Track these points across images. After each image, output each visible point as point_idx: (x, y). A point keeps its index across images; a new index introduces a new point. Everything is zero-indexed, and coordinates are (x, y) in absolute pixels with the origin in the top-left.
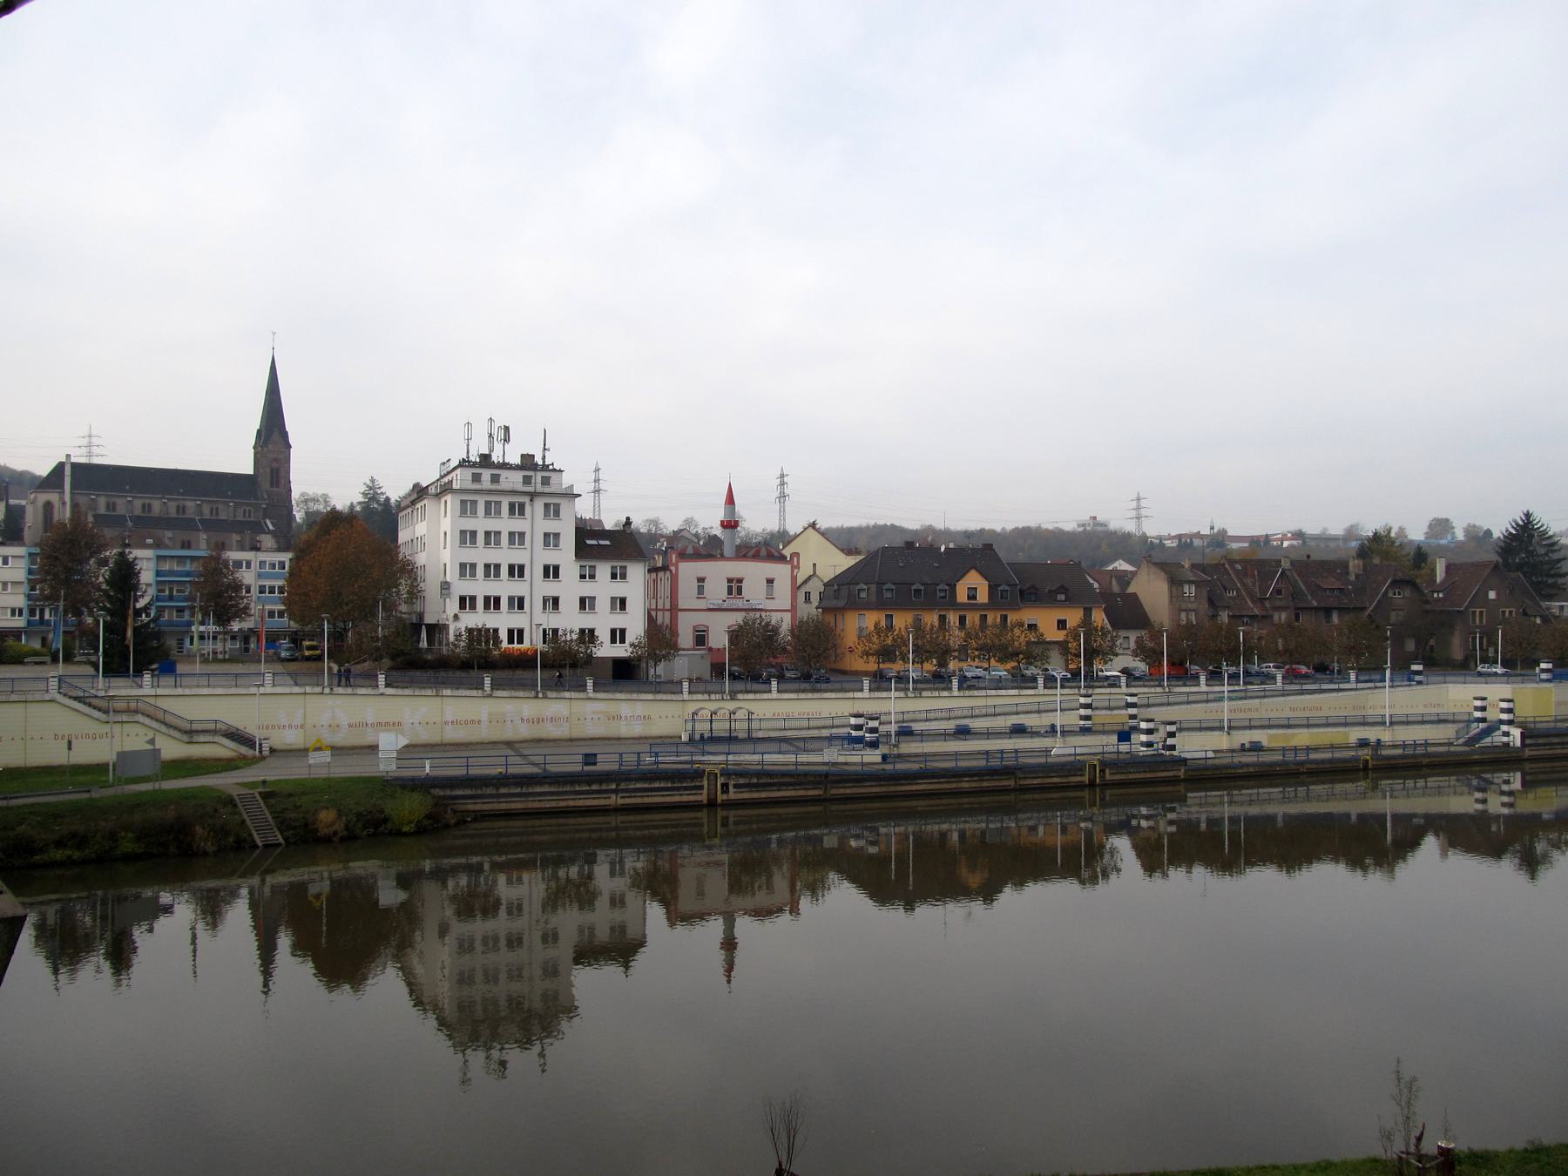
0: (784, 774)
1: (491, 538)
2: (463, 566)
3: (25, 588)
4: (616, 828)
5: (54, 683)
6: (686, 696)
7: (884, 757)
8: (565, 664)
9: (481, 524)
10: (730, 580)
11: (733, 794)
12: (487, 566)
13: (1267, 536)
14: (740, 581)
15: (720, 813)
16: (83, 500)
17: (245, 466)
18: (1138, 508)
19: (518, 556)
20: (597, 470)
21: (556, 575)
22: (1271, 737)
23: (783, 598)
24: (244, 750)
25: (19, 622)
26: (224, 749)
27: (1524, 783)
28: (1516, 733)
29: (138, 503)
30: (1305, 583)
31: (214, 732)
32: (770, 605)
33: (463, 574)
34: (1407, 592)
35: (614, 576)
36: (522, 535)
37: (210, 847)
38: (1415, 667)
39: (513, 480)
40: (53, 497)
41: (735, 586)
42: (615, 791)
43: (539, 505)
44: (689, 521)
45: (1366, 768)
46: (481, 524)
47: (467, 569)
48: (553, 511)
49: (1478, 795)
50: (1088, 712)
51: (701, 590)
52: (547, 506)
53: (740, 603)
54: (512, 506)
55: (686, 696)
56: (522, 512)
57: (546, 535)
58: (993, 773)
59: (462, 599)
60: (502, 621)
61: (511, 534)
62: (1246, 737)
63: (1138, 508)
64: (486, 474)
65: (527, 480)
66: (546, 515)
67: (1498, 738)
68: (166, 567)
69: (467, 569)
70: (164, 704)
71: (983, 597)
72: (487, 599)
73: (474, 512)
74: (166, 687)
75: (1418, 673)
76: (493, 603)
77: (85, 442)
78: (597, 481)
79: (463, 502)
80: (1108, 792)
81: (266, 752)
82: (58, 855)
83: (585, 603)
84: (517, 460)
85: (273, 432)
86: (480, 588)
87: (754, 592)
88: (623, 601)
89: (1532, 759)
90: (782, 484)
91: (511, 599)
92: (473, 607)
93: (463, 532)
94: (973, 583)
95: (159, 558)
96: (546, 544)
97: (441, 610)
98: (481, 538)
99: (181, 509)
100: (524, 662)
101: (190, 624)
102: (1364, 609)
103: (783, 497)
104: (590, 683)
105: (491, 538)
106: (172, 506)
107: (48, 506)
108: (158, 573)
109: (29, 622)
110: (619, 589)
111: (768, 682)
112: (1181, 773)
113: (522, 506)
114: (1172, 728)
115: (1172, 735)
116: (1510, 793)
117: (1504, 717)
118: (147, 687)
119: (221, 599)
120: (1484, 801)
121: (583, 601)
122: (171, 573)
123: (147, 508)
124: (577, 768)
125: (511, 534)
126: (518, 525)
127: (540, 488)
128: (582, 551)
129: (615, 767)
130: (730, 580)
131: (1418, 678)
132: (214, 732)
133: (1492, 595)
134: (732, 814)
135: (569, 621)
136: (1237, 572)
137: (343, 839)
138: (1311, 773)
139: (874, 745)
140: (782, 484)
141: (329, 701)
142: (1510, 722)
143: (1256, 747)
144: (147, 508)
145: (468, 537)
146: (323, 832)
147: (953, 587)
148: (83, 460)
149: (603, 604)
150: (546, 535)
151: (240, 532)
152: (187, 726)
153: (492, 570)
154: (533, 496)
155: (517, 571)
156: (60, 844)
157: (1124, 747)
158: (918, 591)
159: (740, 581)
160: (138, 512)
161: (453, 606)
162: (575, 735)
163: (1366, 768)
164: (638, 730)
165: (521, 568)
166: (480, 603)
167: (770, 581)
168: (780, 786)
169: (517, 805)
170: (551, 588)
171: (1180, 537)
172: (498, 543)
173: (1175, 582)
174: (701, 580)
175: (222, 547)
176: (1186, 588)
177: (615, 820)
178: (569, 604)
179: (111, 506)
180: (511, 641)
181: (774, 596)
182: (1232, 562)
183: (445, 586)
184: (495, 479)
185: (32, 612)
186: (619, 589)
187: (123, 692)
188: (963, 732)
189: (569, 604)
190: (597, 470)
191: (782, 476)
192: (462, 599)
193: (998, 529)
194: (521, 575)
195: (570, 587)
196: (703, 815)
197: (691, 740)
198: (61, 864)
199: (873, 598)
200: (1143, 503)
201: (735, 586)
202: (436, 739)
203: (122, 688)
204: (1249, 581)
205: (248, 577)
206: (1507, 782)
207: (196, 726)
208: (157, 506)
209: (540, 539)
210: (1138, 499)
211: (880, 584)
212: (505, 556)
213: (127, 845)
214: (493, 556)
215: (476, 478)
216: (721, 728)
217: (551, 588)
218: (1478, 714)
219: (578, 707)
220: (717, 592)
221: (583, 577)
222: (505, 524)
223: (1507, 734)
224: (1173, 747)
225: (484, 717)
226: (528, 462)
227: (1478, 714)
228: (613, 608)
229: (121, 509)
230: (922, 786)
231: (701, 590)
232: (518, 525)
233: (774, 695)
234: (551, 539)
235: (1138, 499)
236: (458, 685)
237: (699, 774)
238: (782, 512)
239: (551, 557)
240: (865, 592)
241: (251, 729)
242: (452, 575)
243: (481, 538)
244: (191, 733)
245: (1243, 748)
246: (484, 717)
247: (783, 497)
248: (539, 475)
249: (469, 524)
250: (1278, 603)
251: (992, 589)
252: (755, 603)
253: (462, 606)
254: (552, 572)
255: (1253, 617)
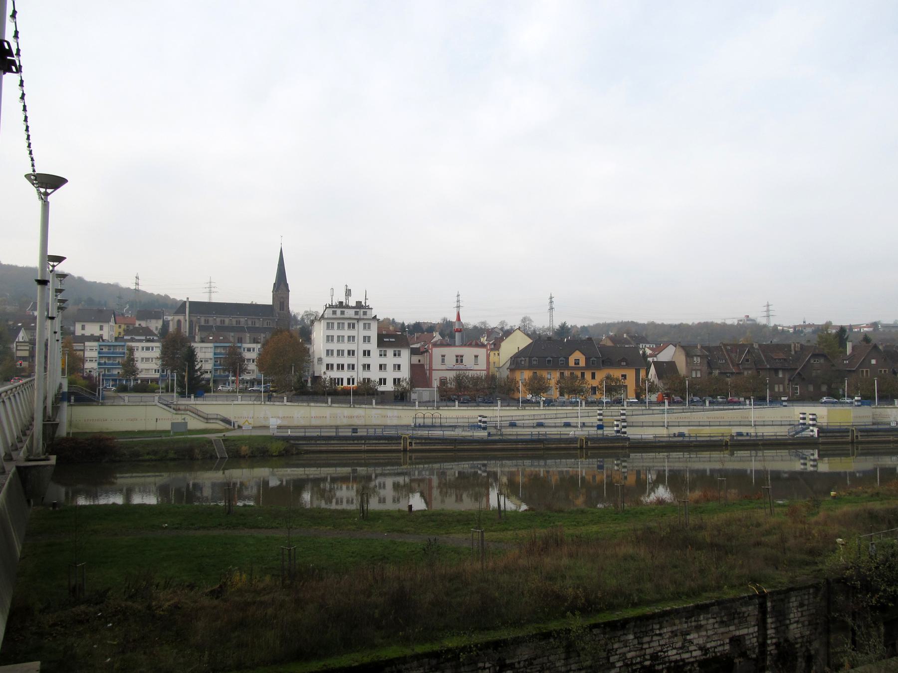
0: (436, 439)
1: (340, 339)
2: (328, 351)
3: (213, 361)
4: (364, 459)
5: (157, 398)
6: (417, 408)
7: (489, 434)
8: (366, 393)
9: (335, 333)
10: (457, 356)
11: (414, 447)
12: (338, 351)
13: (851, 326)
14: (462, 356)
15: (409, 454)
16: (194, 319)
17: (271, 303)
18: (768, 311)
19: (352, 347)
20: (458, 296)
21: (369, 355)
22: (689, 430)
23: (482, 365)
24: (227, 426)
25: (157, 375)
26: (220, 425)
27: (819, 455)
28: (816, 430)
29: (218, 320)
30: (765, 356)
31: (216, 419)
32: (476, 367)
33: (328, 354)
34: (822, 361)
35: (395, 355)
36: (354, 337)
37: (199, 457)
38: (783, 398)
39: (350, 313)
40: (181, 318)
41: (459, 359)
42: (364, 444)
43: (361, 324)
44: (502, 323)
45: (726, 445)
46: (335, 333)
47: (329, 353)
48: (367, 327)
49: (802, 461)
50: (601, 417)
51: (443, 361)
52: (365, 324)
53: (461, 367)
54: (349, 324)
55: (417, 408)
56: (354, 327)
57: (365, 337)
58: (532, 441)
59: (328, 365)
60: (345, 375)
61: (349, 337)
62: (676, 430)
63: (768, 311)
64: (339, 311)
65: (356, 313)
66: (365, 328)
67: (807, 433)
68: (218, 351)
69: (329, 353)
70: (198, 408)
71: (582, 363)
72: (338, 365)
73: (333, 328)
74: (200, 401)
75: (784, 401)
76: (341, 367)
77: (208, 285)
78: (458, 301)
79: (328, 324)
80: (589, 452)
81: (236, 426)
82: (147, 457)
83: (382, 367)
84: (354, 304)
85: (281, 285)
86: (335, 360)
87: (468, 362)
88: (399, 366)
89: (823, 444)
90: (551, 302)
91: (349, 365)
92: (332, 368)
93: (328, 336)
94: (577, 357)
95: (215, 347)
96: (364, 341)
97: (320, 370)
98: (335, 339)
99: (238, 322)
100: (346, 392)
101: (228, 376)
102: (796, 369)
103: (551, 309)
104: (374, 401)
105: (340, 339)
106: (234, 321)
107: (179, 322)
108: (215, 354)
109: (162, 376)
110: (397, 361)
111: (454, 401)
112: (627, 444)
113: (354, 325)
114: (625, 424)
115: (624, 427)
116: (814, 460)
117: (811, 422)
118: (192, 401)
119: (233, 363)
120: (805, 464)
121: (381, 366)
122: (220, 354)
123: (223, 322)
124: (350, 434)
125: (349, 337)
126: (352, 333)
127: (362, 317)
128: (381, 343)
129: (365, 434)
130: (457, 356)
131: (784, 404)
132: (216, 419)
133: (873, 362)
134: (414, 455)
135: (374, 375)
136: (727, 351)
137: (250, 457)
138: (695, 446)
139: (485, 428)
140: (551, 302)
141: (264, 407)
142: (813, 425)
143: (682, 435)
144: (223, 322)
145: (329, 339)
146: (243, 454)
147: (567, 359)
148: (205, 299)
149: (390, 367)
150: (365, 337)
151: (264, 333)
152: (206, 416)
153: (340, 353)
154: (358, 320)
155: (351, 353)
156: (148, 454)
157: (600, 432)
158: (549, 361)
159: (462, 356)
160: (218, 324)
161: (324, 368)
162: (367, 423)
163: (726, 445)
164: (395, 422)
165: (353, 351)
166: (335, 367)
167: (476, 357)
168: (435, 444)
169: (324, 448)
170: (366, 361)
171: (795, 327)
172: (343, 341)
173: (689, 355)
174: (443, 356)
175: (240, 340)
176: (695, 359)
177: (363, 456)
178: (375, 367)
179: (207, 321)
180: (349, 383)
181: (476, 362)
182: (725, 345)
183: (320, 360)
184: (342, 313)
185: (163, 371)
186: (397, 361)
187: (184, 402)
188: (540, 425)
189: (375, 367)
190: (458, 296)
191: (551, 298)
192: (328, 365)
193: (690, 323)
194: (353, 354)
195: (375, 360)
196: (401, 454)
197: (415, 426)
198: (148, 460)
199: (527, 364)
200: (771, 308)
201: (459, 359)
202: (307, 424)
203: (184, 401)
204: (733, 355)
205: (247, 355)
206: (813, 455)
207: (210, 416)
208: (227, 321)
209: (361, 339)
210: (768, 306)
211: (530, 358)
212: (346, 346)
213: (171, 455)
214: (341, 346)
215: (334, 313)
216: (428, 422)
217: (366, 361)
218: (801, 421)
219: (368, 411)
220: (451, 361)
221: (381, 355)
222: (346, 333)
223: (812, 431)
224: (625, 433)
225: (328, 416)
226: (359, 304)
227: (801, 421)
228: (394, 369)
229: (211, 323)
230: (499, 446)
231: (443, 361)
232: (352, 333)
233: (457, 408)
234: (367, 339)
235: (768, 306)
236: (317, 401)
237: (399, 438)
238: (551, 316)
239: (367, 347)
240: (524, 361)
241: (233, 420)
242: (323, 355)
243: (335, 339)
244: (207, 419)
245: (675, 435)
246: (328, 416)
247: (551, 309)
248: (362, 311)
249: (330, 333)
250: (747, 366)
251: (587, 360)
252: (468, 367)
253: (328, 368)
254: (367, 353)
255: (732, 373)
